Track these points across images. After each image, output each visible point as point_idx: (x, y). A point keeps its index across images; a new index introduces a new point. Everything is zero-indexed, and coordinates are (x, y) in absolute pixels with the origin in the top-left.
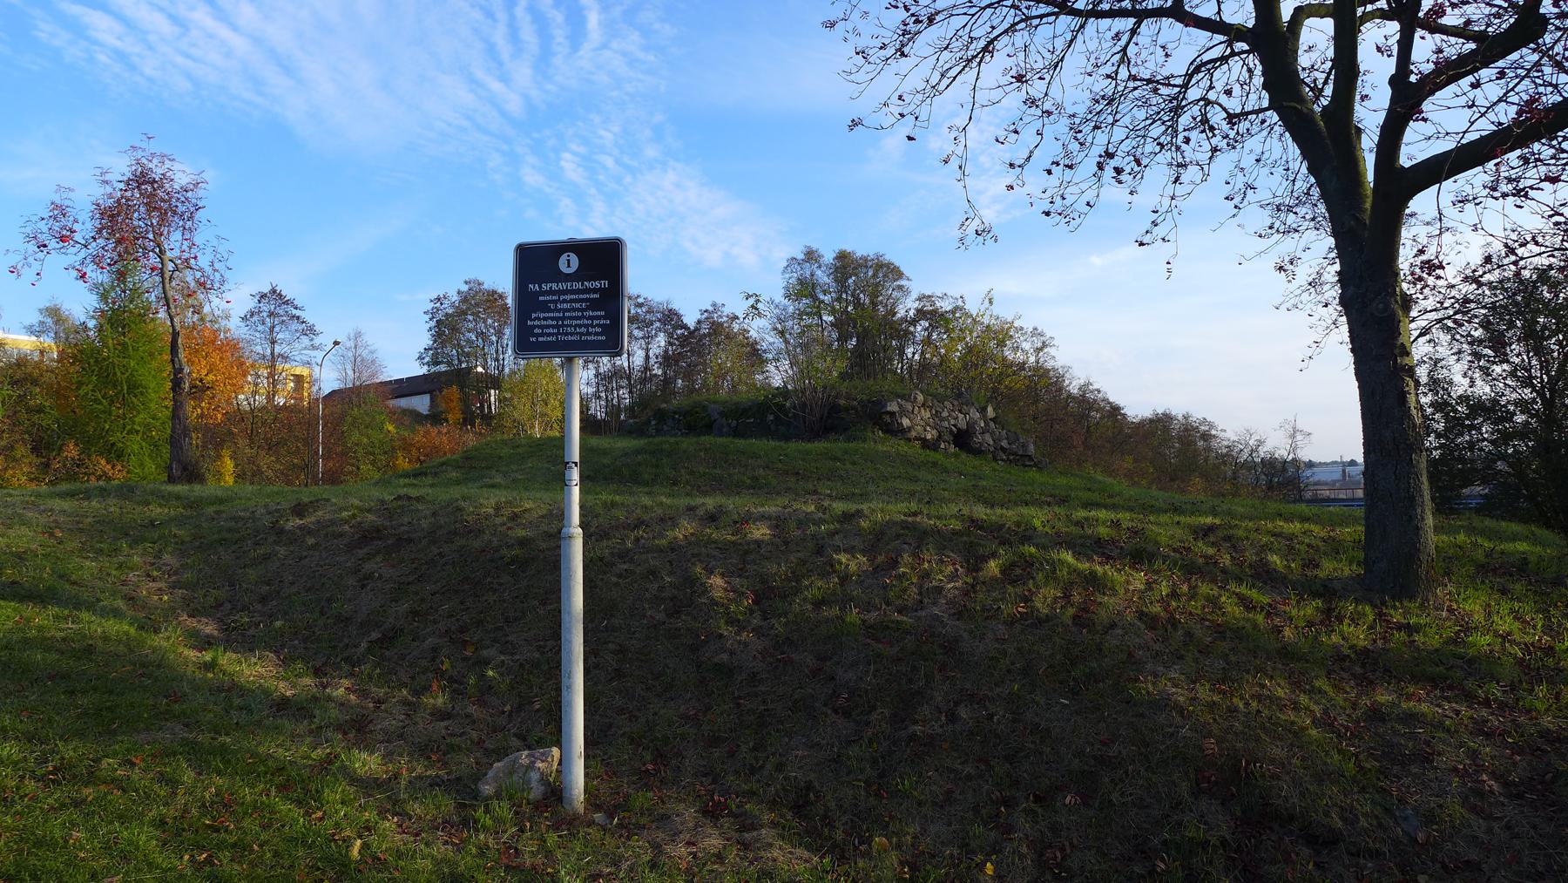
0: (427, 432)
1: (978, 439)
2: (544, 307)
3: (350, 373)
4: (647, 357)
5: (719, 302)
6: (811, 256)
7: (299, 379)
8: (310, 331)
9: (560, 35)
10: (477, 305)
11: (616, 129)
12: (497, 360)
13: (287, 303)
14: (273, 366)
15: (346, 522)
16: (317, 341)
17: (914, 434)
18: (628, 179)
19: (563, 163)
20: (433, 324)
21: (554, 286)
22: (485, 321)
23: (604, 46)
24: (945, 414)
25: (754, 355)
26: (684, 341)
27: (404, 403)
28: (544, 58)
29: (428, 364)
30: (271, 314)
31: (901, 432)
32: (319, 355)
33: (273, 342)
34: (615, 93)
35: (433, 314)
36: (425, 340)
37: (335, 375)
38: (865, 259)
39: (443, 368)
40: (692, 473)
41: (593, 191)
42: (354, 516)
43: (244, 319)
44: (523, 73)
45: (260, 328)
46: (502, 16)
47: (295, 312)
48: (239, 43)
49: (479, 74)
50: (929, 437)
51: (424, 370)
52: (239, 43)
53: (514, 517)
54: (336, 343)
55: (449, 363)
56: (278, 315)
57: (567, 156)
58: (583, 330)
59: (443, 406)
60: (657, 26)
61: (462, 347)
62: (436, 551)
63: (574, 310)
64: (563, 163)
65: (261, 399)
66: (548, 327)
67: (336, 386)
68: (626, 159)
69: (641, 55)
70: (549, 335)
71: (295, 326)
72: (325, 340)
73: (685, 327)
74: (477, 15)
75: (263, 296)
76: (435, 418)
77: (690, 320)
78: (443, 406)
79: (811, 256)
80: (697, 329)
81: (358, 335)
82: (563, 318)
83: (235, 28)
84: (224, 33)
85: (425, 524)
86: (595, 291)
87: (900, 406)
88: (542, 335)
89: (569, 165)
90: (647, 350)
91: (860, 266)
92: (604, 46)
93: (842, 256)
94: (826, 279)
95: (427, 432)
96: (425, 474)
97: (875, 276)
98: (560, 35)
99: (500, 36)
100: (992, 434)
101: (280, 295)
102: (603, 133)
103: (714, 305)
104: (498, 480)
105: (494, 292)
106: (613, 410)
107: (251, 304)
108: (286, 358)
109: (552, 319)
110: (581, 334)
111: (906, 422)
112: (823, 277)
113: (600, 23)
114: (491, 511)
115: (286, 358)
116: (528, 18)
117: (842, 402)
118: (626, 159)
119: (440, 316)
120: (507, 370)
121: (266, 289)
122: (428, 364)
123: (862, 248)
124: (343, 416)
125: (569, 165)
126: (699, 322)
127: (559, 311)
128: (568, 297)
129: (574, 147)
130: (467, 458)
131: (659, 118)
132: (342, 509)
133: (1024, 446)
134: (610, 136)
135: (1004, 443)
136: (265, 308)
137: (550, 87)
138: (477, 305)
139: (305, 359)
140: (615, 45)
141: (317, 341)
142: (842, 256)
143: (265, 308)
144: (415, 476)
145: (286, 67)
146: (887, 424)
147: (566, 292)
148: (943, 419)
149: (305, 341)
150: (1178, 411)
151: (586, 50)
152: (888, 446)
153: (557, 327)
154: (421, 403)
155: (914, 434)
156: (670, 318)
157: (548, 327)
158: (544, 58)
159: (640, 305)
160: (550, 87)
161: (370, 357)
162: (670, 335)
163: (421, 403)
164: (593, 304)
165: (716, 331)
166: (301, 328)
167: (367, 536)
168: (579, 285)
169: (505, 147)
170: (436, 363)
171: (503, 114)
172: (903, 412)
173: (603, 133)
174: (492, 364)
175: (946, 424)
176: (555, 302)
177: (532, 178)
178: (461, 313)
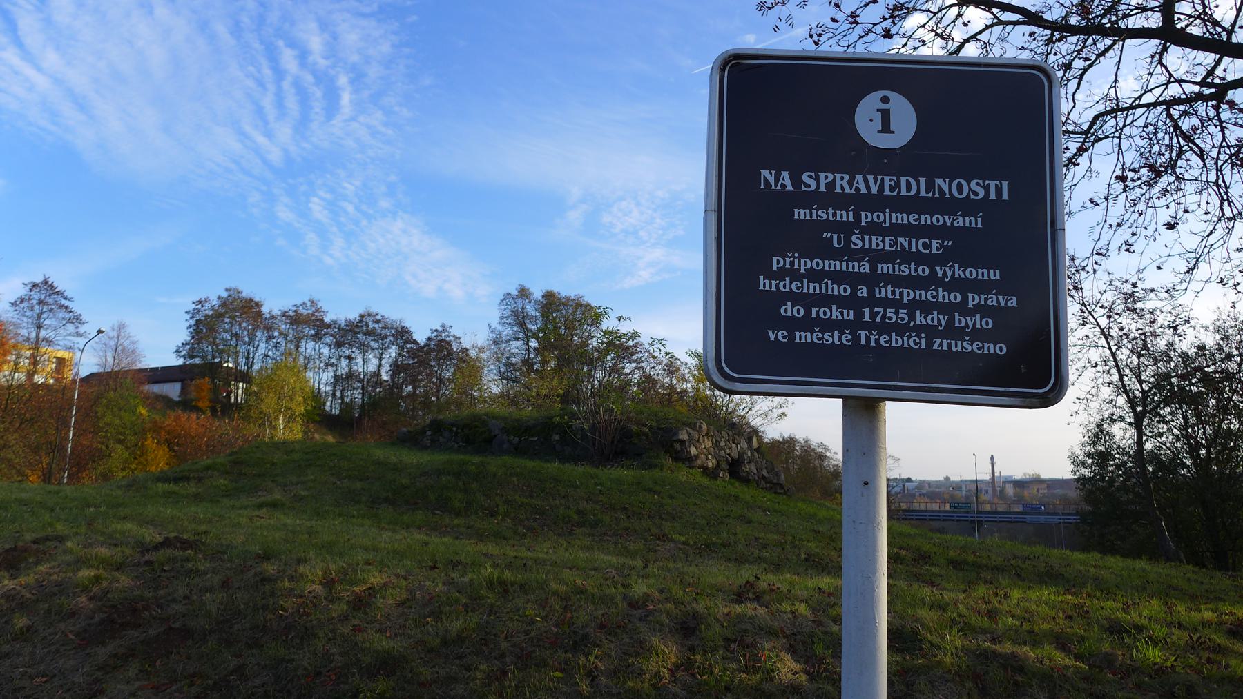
0: (178, 418)
1: (746, 468)
2: (812, 241)
3: (110, 359)
4: (380, 366)
5: (448, 324)
6: (523, 293)
7: (61, 362)
8: (76, 320)
9: (318, 107)
10: (235, 310)
11: (358, 183)
12: (247, 358)
13: (57, 293)
14: (36, 348)
15: (85, 589)
16: (82, 329)
17: (699, 462)
18: (364, 222)
19: (311, 205)
20: (192, 322)
21: (841, 183)
22: (240, 325)
23: (353, 119)
24: (722, 444)
25: (467, 365)
26: (413, 354)
27: (157, 389)
28: (302, 124)
29: (184, 356)
30: (40, 302)
31: (689, 460)
32: (82, 341)
33: (39, 327)
34: (359, 156)
35: (193, 314)
36: (183, 335)
37: (95, 360)
38: (568, 299)
39: (197, 361)
40: (507, 502)
41: (334, 229)
42: (97, 579)
43: (14, 304)
44: (284, 132)
45: (29, 313)
46: (271, 88)
47: (63, 302)
48: (41, 81)
49: (248, 128)
50: (710, 465)
51: (180, 362)
52: (41, 81)
53: (360, 603)
54: (100, 332)
55: (203, 358)
56: (47, 303)
57: (315, 200)
58: (935, 319)
59: (193, 395)
60: (396, 109)
61: (217, 345)
62: (233, 663)
63: (906, 257)
64: (311, 205)
65: (20, 377)
66: (825, 300)
67: (95, 370)
68: (364, 207)
69: (383, 129)
70: (829, 326)
71: (62, 314)
72: (90, 329)
73: (415, 342)
74: (250, 83)
75: (35, 286)
76: (186, 404)
77: (421, 336)
78: (193, 395)
79: (523, 293)
80: (426, 345)
81: (122, 327)
82: (872, 280)
83: (39, 69)
84: (29, 72)
85: (213, 602)
86: (968, 206)
87: (689, 435)
88: (807, 324)
89: (317, 207)
90: (381, 359)
91: (564, 304)
92: (353, 119)
93: (549, 296)
94: (533, 313)
95: (178, 418)
96: (188, 479)
97: (574, 313)
98: (318, 107)
99: (268, 102)
100: (756, 463)
101: (51, 286)
102: (346, 185)
103: (443, 326)
104: (277, 495)
105: (251, 300)
106: (347, 407)
107: (22, 291)
108: (49, 342)
109: (838, 278)
110: (931, 332)
111: (693, 450)
112: (531, 310)
113: (351, 101)
114: (318, 588)
115: (49, 342)
116: (293, 91)
117: (634, 428)
118: (364, 207)
119: (198, 317)
120: (256, 367)
121: (39, 279)
122: (184, 356)
123: (565, 290)
124: (97, 400)
125: (317, 207)
126: (429, 339)
127: (858, 255)
128: (887, 218)
129: (322, 193)
130: (235, 463)
131: (393, 178)
132: (81, 562)
133: (777, 475)
134: (352, 188)
135: (764, 472)
136: (35, 295)
137: (305, 145)
138: (235, 310)
139: (69, 344)
140: (361, 119)
141: (82, 329)
142: (549, 296)
143: (35, 295)
144: (176, 480)
145: (81, 104)
146: (677, 452)
147: (878, 202)
148: (721, 449)
149: (71, 328)
150: (800, 436)
151: (337, 121)
152: (684, 475)
153: (850, 302)
154: (173, 390)
155: (699, 462)
156: (403, 334)
157: (825, 300)
158: (302, 124)
159: (378, 322)
160: (305, 145)
161: (131, 347)
162: (402, 348)
163: (173, 390)
164: (964, 248)
165: (441, 347)
166: (68, 316)
167: (117, 617)
168: (919, 187)
169: (264, 188)
170: (192, 357)
171: (265, 162)
172: (692, 441)
173: (346, 185)
174: (242, 360)
175: (723, 453)
176: (845, 229)
177: (284, 214)
178: (218, 315)
